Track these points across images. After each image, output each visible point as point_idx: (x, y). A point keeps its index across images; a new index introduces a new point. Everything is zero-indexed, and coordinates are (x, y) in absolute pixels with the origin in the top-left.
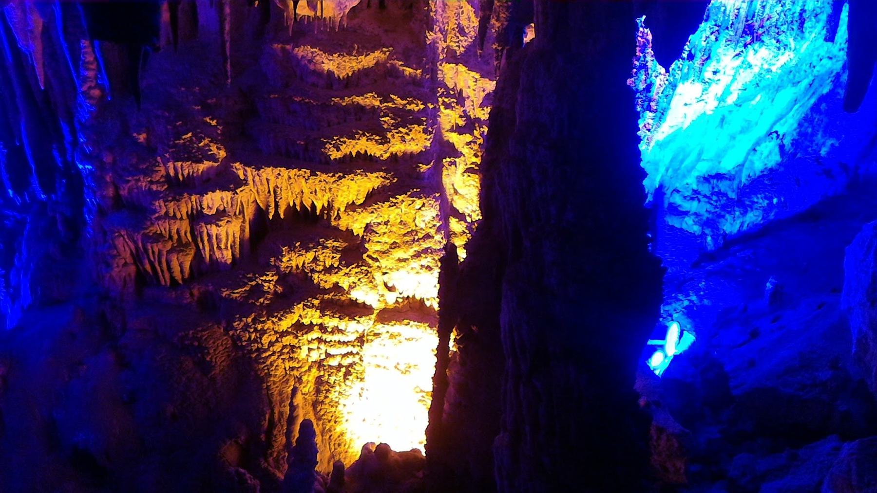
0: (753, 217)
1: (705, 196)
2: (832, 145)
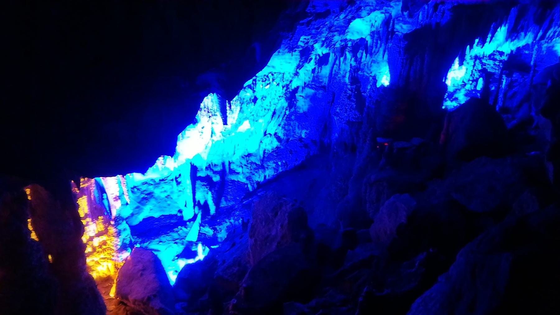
0: (269, 173)
1: (245, 165)
2: (306, 133)
